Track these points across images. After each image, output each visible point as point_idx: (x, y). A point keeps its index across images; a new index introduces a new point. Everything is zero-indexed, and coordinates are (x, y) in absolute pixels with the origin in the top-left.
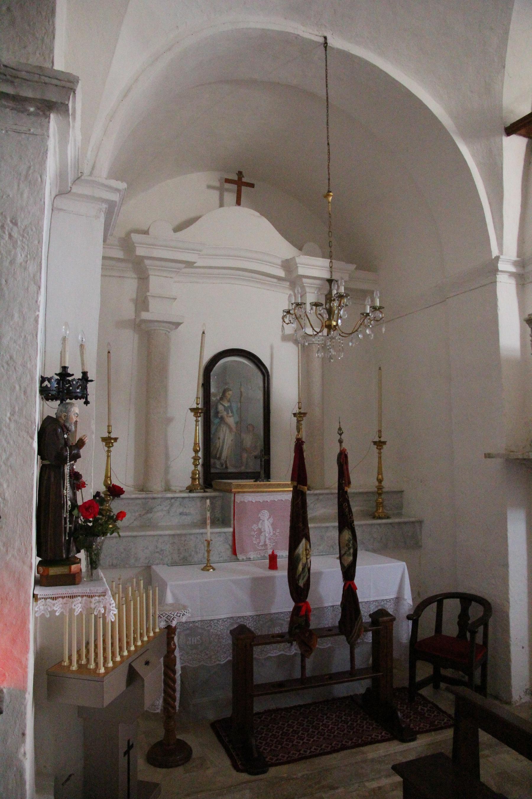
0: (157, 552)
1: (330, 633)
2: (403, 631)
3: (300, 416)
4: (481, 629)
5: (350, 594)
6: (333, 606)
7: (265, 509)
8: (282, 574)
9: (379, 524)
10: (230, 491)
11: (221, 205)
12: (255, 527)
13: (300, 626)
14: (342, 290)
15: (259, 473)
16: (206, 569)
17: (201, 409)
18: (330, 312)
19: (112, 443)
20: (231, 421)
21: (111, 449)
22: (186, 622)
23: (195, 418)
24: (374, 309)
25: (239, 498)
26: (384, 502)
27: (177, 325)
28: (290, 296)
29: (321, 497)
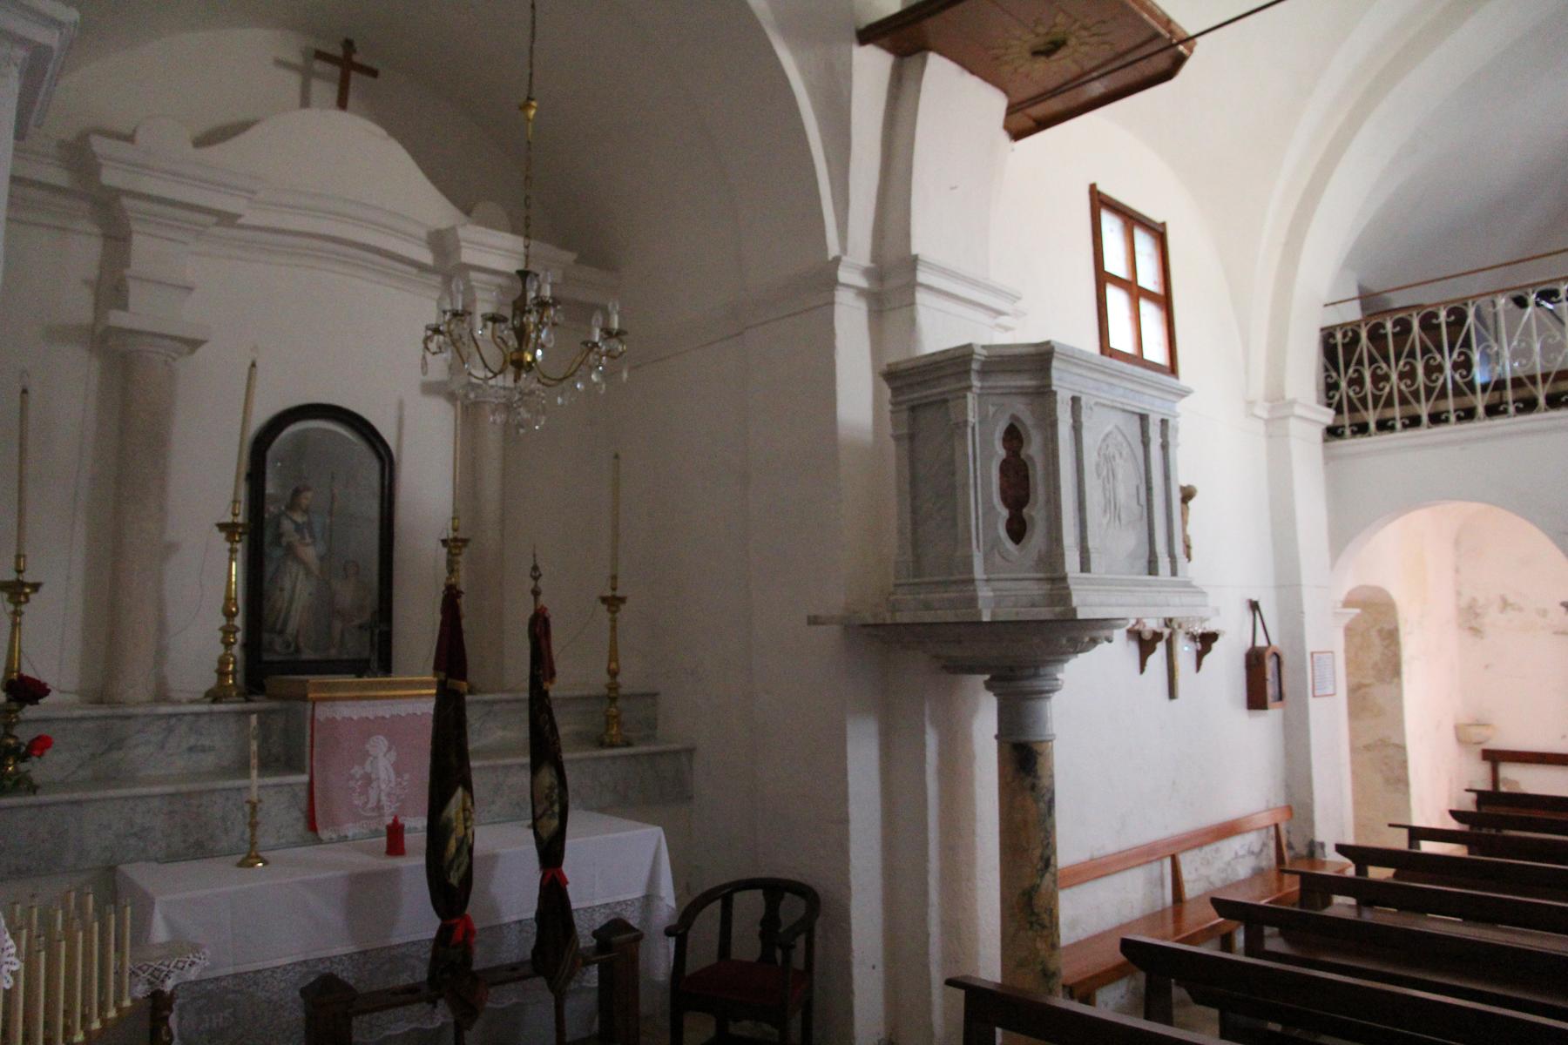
0: (135, 834)
1: (516, 975)
2: (659, 959)
3: (454, 545)
4: (801, 941)
5: (553, 893)
6: (520, 922)
7: (378, 738)
8: (414, 862)
9: (613, 758)
10: (304, 698)
11: (305, 102)
12: (357, 771)
13: (453, 968)
14: (547, 292)
15: (368, 661)
16: (247, 863)
17: (242, 525)
18: (521, 334)
19: (26, 595)
20: (310, 553)
21: (24, 608)
22: (197, 983)
23: (228, 545)
24: (608, 333)
25: (323, 712)
26: (620, 716)
27: (194, 344)
28: (441, 299)
29: (496, 708)
